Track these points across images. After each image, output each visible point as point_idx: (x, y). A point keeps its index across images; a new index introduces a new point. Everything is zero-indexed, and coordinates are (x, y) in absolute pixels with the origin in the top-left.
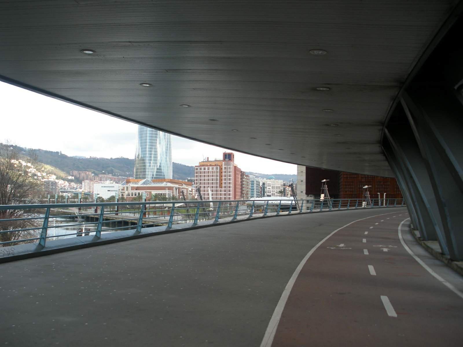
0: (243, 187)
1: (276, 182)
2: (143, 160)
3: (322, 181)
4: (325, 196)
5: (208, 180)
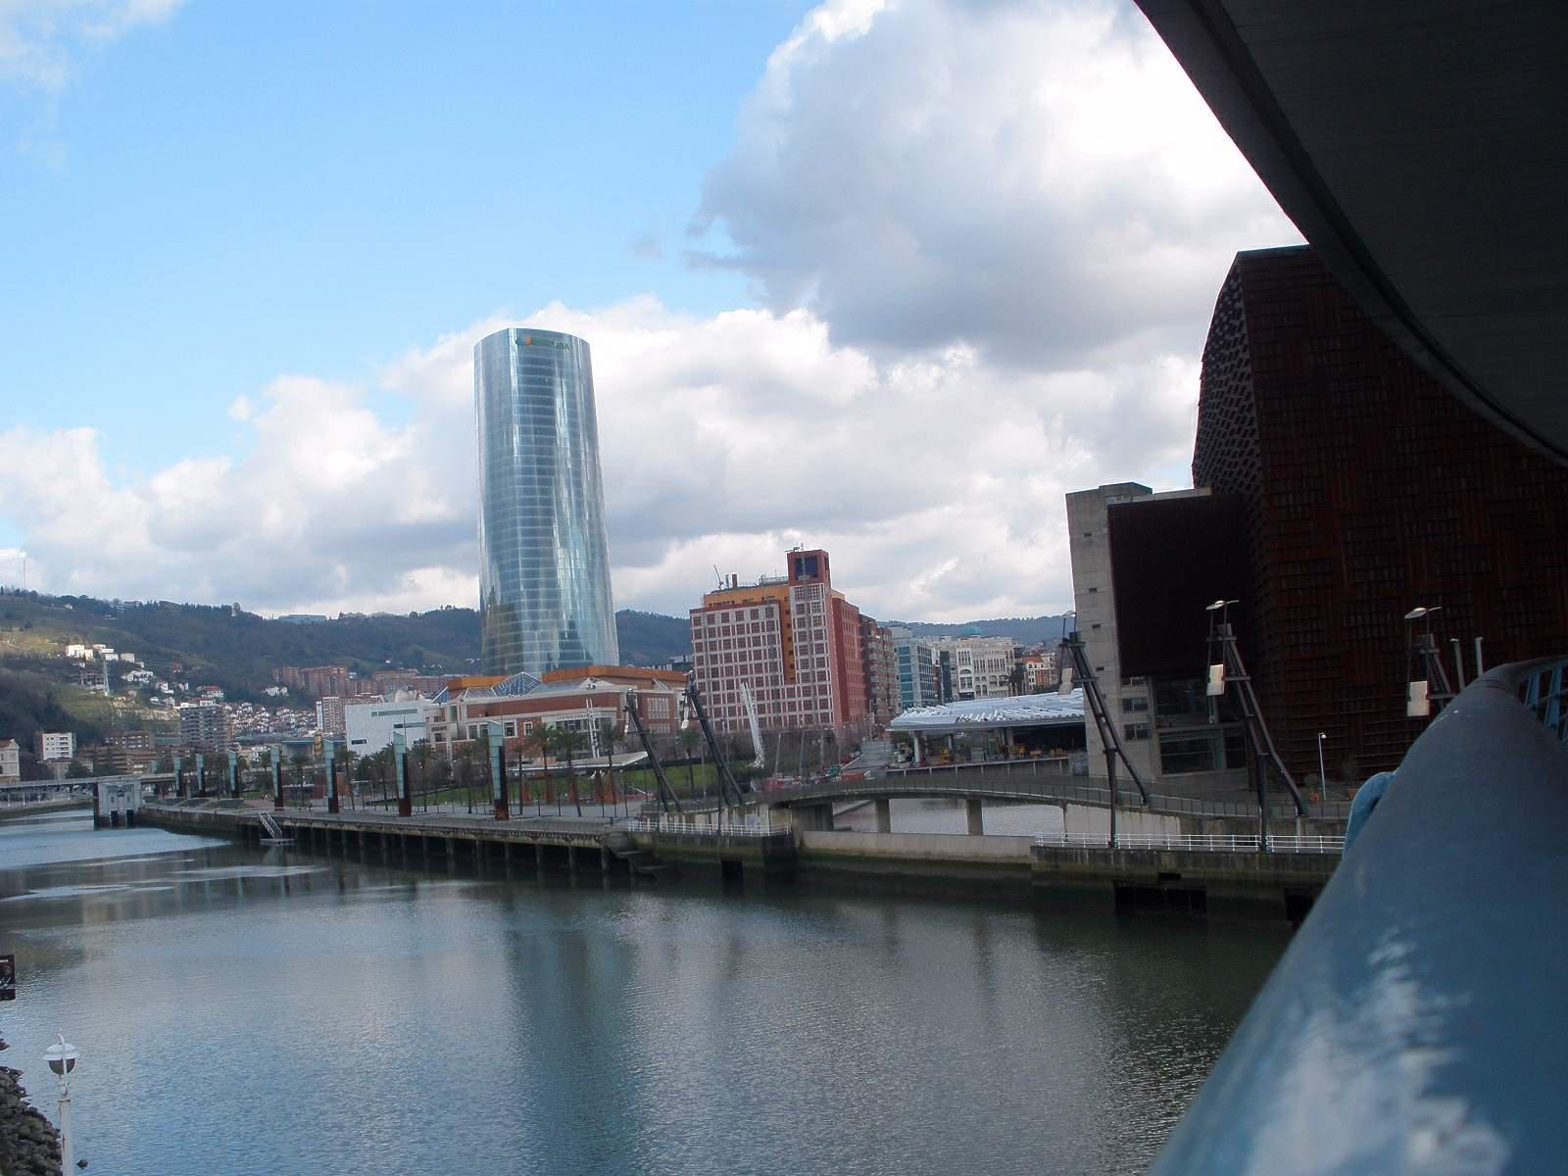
0: (873, 674)
1: (990, 646)
2: (511, 607)
3: (1208, 608)
4: (1227, 672)
5: (743, 657)
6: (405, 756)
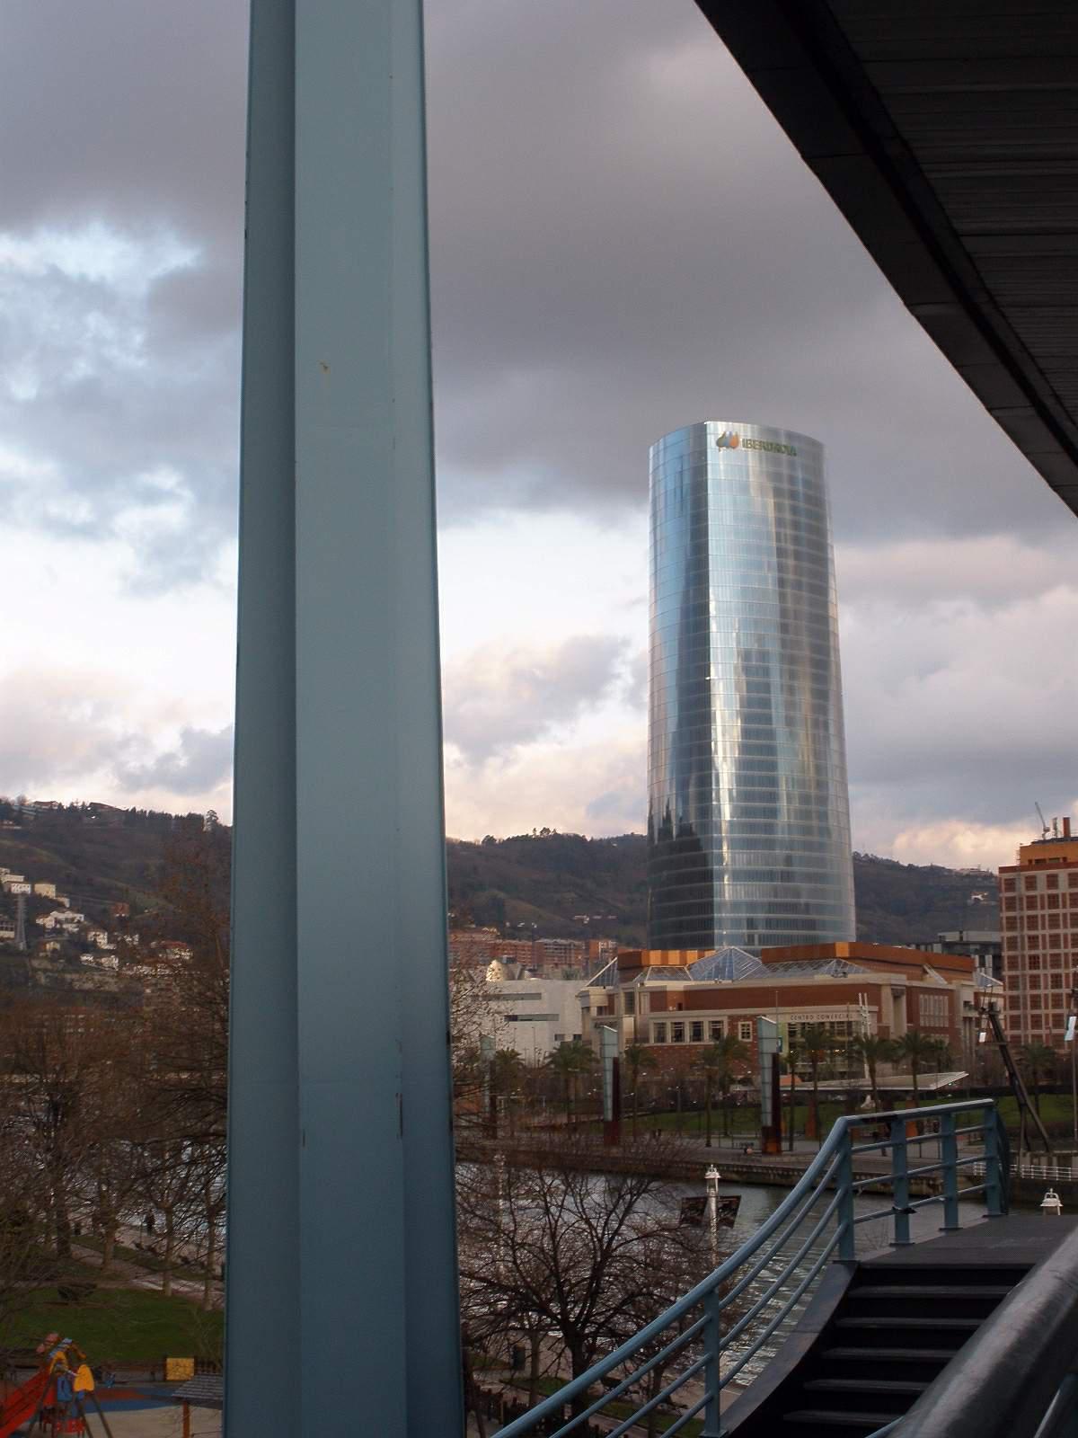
6: (616, 1062)
